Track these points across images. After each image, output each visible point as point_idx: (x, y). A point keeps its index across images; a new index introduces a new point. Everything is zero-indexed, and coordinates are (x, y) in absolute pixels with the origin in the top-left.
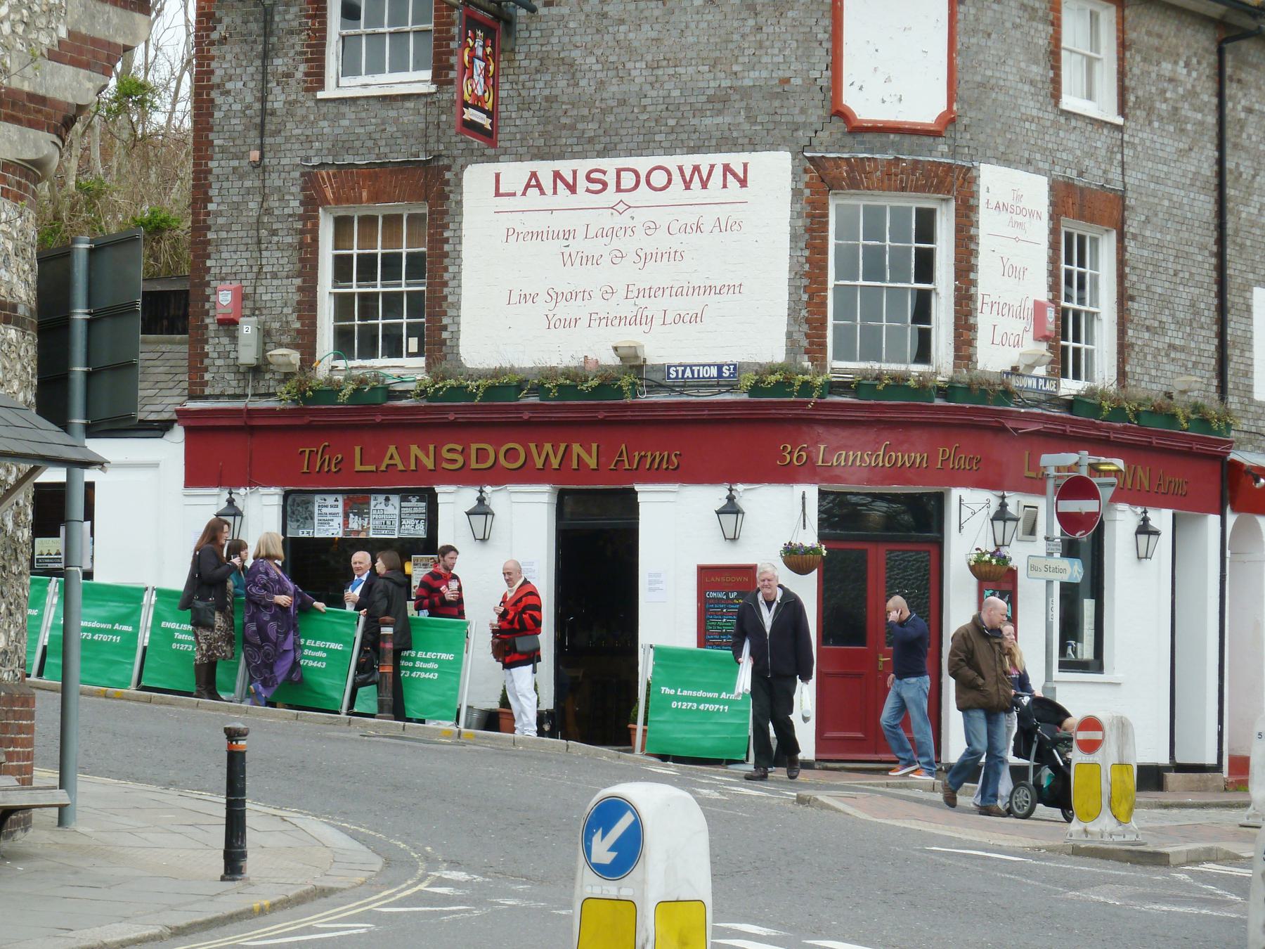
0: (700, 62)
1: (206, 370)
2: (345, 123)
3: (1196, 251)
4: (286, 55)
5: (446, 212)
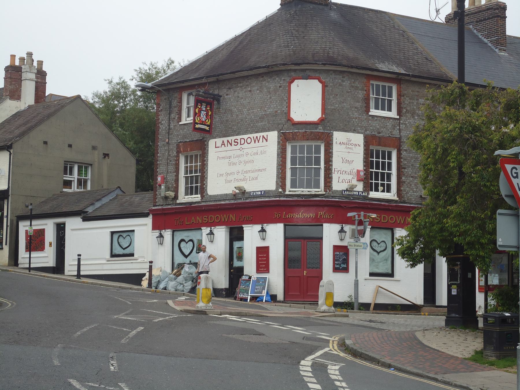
5: (205, 153)
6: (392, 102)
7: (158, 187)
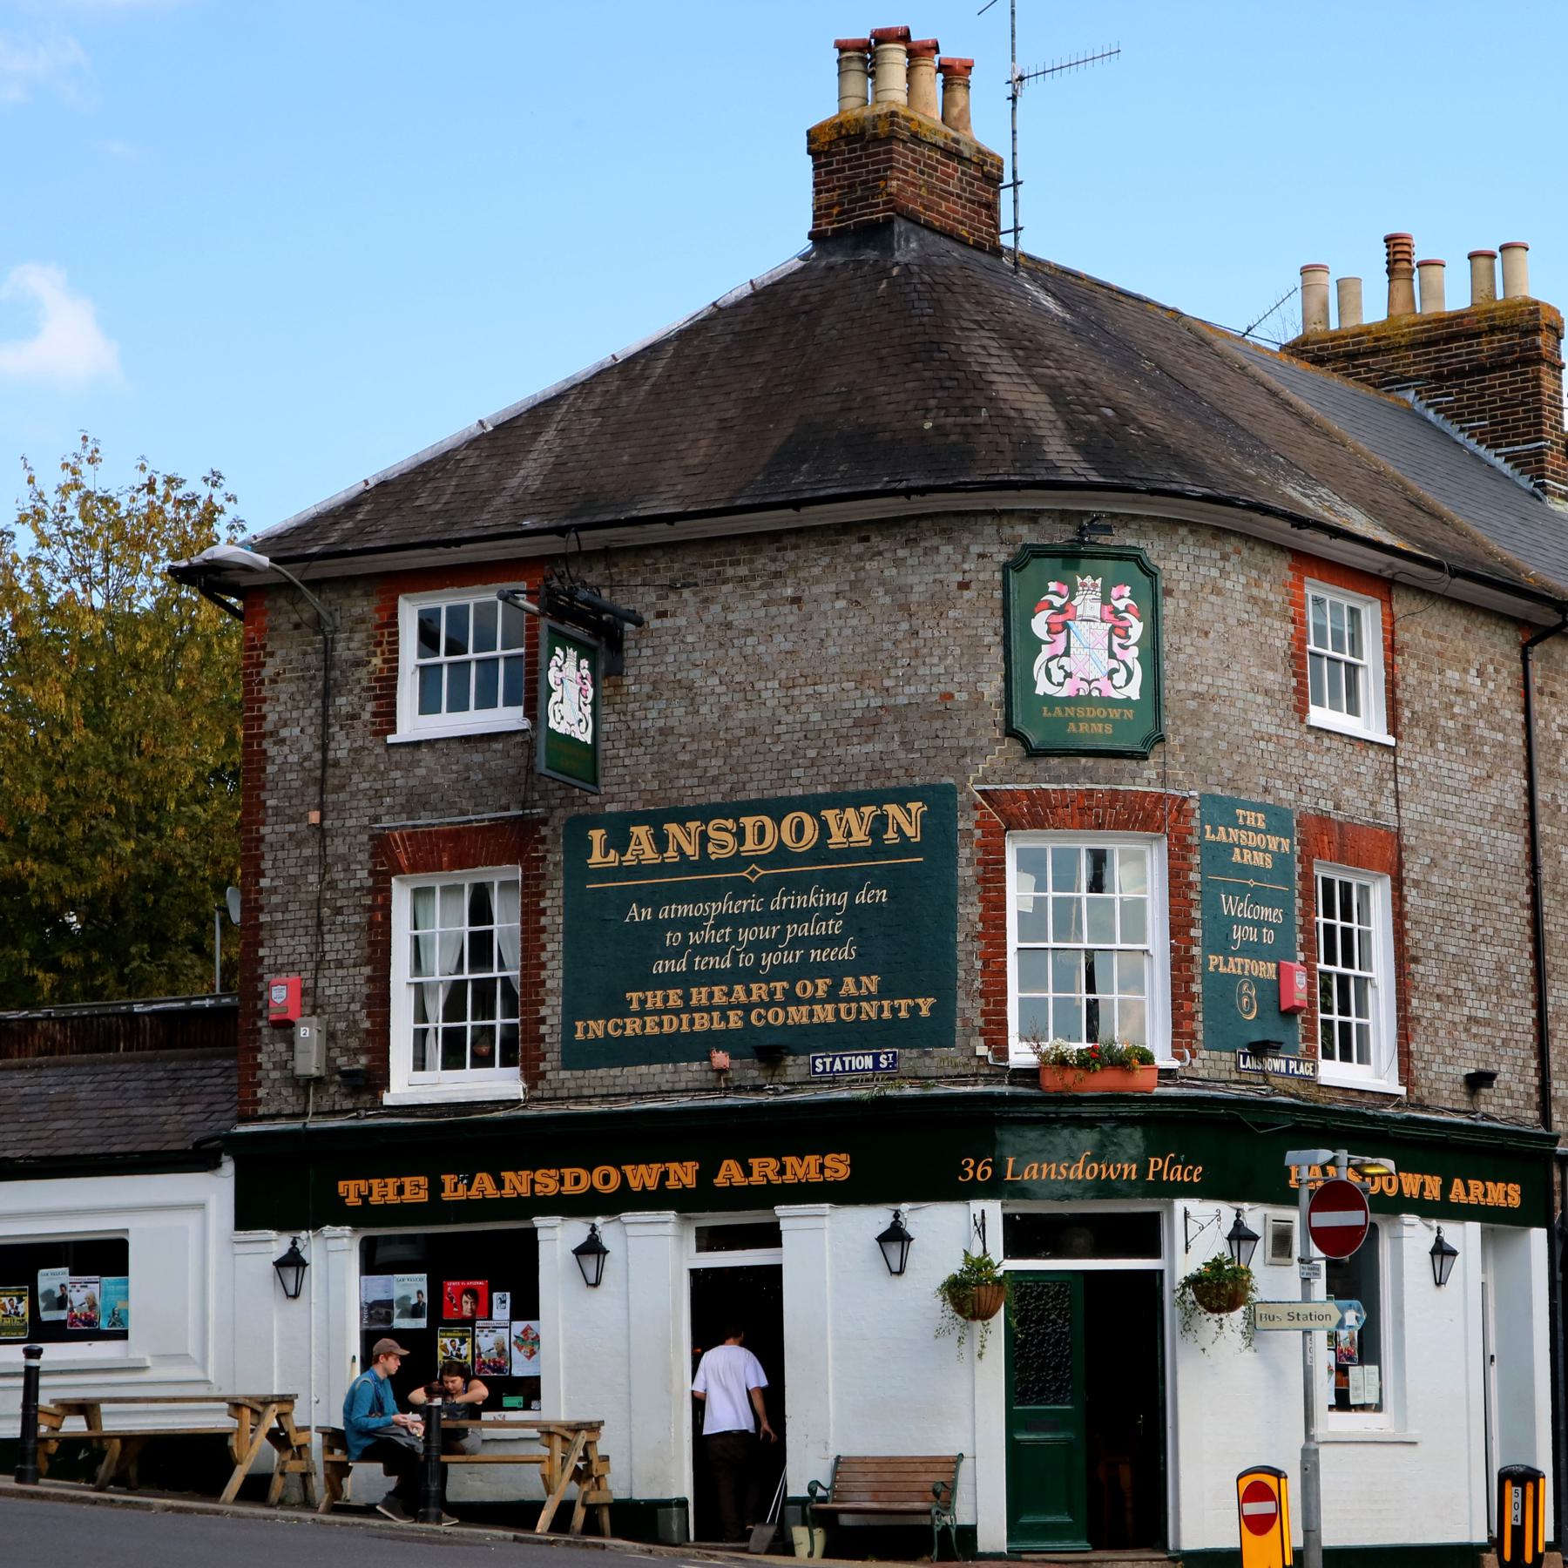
0: (844, 677)
1: (259, 1085)
2: (422, 772)
3: (1502, 901)
4: (351, 691)
6: (1361, 673)
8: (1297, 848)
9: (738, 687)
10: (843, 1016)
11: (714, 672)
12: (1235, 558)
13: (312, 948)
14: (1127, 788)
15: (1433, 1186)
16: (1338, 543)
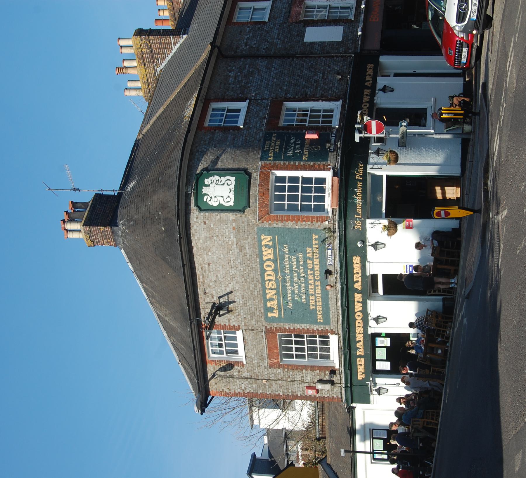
2: (253, 356)
7: (319, 395)
8: (275, 131)
9: (231, 279)
10: (317, 257)
11: (228, 285)
12: (198, 148)
13: (298, 383)
14: (258, 182)
15: (367, 92)
16: (194, 118)
